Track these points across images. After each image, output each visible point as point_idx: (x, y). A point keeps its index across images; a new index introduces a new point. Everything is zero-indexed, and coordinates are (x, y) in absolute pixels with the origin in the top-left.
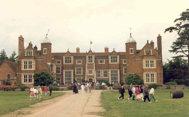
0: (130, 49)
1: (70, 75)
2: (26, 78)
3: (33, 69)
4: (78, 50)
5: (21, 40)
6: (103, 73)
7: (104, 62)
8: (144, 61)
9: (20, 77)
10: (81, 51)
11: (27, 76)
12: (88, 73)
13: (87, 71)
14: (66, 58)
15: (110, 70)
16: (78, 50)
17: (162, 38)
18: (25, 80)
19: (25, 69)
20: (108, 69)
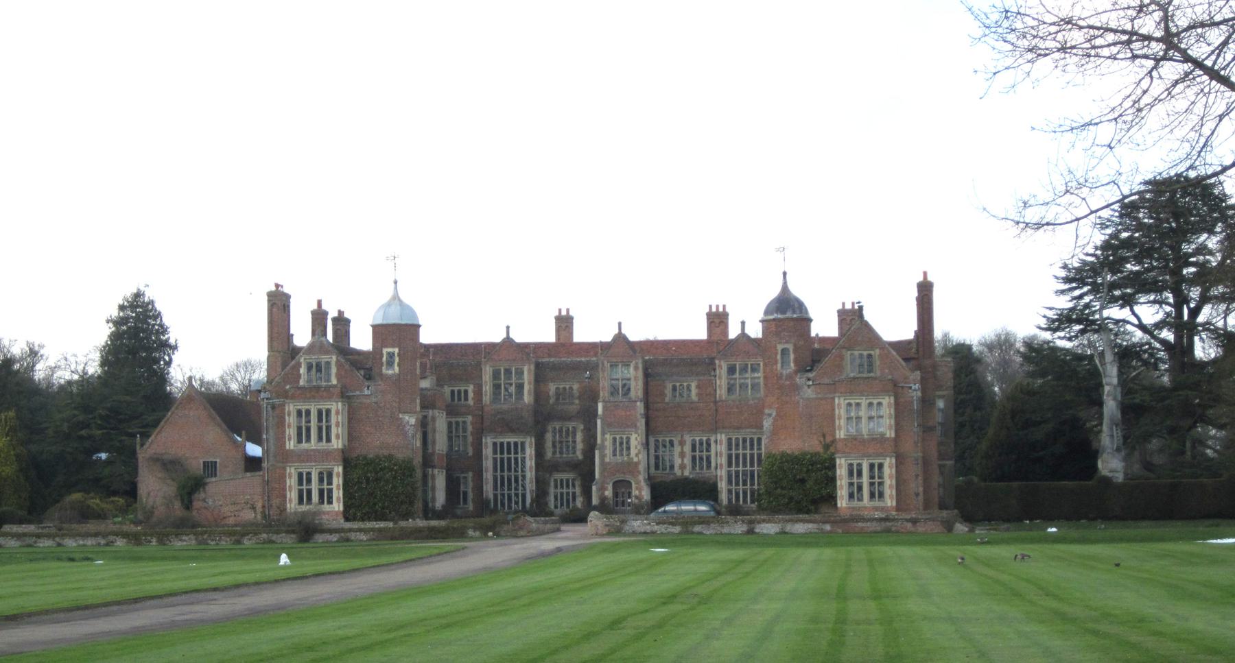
0: (780, 347)
1: (516, 463)
2: (304, 487)
3: (337, 444)
4: (564, 323)
5: (279, 304)
6: (688, 448)
7: (694, 391)
8: (840, 402)
9: (283, 478)
10: (581, 335)
11: (309, 474)
12: (609, 451)
13: (605, 439)
14: (496, 375)
15: (722, 437)
16: (564, 323)
17: (351, 324)
18: (300, 492)
19: (304, 445)
20: (715, 430)
